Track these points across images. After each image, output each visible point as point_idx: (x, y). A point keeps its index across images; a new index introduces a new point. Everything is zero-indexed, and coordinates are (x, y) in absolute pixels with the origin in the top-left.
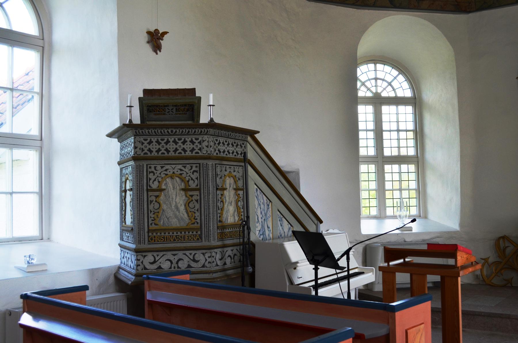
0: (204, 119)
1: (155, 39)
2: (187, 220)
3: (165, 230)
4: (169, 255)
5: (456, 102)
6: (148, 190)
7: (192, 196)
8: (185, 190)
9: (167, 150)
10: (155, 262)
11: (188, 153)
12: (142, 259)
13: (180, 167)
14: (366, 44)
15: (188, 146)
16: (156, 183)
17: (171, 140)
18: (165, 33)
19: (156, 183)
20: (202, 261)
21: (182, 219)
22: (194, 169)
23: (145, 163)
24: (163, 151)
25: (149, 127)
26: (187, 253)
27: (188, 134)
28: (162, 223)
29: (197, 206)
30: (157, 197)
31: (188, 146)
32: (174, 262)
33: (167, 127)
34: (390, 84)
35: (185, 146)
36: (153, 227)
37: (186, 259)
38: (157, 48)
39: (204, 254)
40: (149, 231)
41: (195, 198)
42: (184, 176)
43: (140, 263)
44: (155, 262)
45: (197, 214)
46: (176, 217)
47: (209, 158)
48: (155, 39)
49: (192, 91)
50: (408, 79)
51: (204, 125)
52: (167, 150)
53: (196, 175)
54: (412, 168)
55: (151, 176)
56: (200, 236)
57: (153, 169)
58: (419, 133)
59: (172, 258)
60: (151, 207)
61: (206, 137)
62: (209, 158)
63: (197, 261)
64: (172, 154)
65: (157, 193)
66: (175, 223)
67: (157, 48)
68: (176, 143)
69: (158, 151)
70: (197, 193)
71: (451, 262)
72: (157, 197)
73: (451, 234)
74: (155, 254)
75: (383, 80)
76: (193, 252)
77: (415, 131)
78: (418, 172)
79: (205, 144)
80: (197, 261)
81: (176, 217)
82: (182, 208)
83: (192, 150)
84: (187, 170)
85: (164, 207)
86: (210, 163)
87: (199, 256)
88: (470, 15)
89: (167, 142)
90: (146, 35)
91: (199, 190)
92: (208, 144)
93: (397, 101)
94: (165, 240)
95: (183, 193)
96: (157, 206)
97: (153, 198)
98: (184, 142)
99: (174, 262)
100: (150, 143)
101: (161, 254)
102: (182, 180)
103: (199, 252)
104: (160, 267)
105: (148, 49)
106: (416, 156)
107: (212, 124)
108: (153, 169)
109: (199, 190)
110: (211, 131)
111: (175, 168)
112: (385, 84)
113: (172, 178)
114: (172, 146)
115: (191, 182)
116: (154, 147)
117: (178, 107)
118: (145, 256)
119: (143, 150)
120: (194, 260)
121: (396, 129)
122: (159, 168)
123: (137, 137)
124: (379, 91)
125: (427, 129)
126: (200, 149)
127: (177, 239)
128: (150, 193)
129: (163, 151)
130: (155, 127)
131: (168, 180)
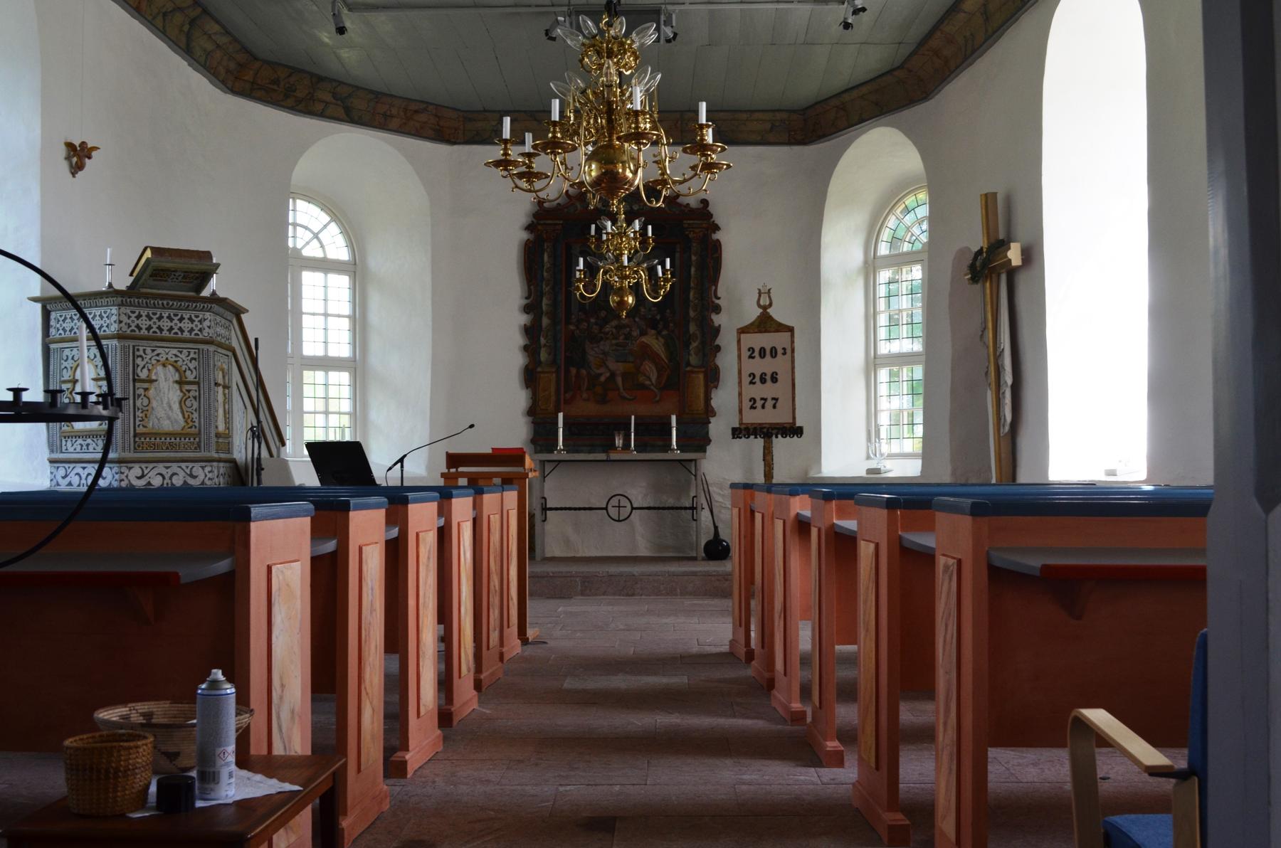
0: (206, 293)
1: (78, 155)
2: (182, 423)
3: (156, 435)
4: (160, 468)
5: (428, 279)
6: (134, 380)
7: (189, 391)
8: (180, 383)
9: (159, 328)
10: (142, 476)
11: (186, 334)
12: (126, 472)
13: (175, 351)
14: (303, 169)
15: (186, 325)
16: (145, 371)
17: (165, 315)
18: (95, 148)
19: (145, 371)
20: (202, 477)
21: (176, 421)
22: (192, 355)
23: (131, 343)
24: (154, 329)
25: (139, 296)
26: (183, 465)
27: (187, 309)
28: (152, 424)
29: (196, 405)
30: (146, 390)
31: (166, 324)
32: (167, 477)
33: (163, 297)
34: (316, 236)
35: (182, 325)
36: (140, 430)
37: (182, 474)
38: (76, 168)
39: (203, 468)
40: (135, 436)
41: (192, 394)
42: (180, 363)
43: (123, 477)
44: (142, 476)
45: (196, 415)
46: (169, 418)
47: (209, 342)
48: (78, 155)
49: (207, 255)
50: (345, 232)
51: (205, 300)
52: (159, 328)
53: (194, 364)
54: (344, 377)
55: (139, 361)
56: (199, 446)
57: (141, 353)
58: (359, 323)
59: (164, 471)
60: (138, 403)
61: (208, 315)
62: (209, 342)
63: (195, 477)
64: (165, 334)
65: (146, 385)
66: (167, 426)
67: (76, 168)
68: (171, 320)
69: (149, 328)
70: (194, 387)
71: (520, 469)
72: (146, 390)
73: (422, 478)
74: (143, 466)
75: (306, 228)
76: (190, 465)
77: (353, 318)
78: (354, 385)
79: (206, 323)
80: (195, 477)
81: (169, 418)
82: (176, 407)
83: (191, 330)
84: (183, 356)
85: (154, 404)
86: (212, 348)
87: (197, 470)
88: (456, 147)
89: (160, 318)
90: (64, 147)
91: (198, 383)
92: (210, 324)
93: (325, 265)
94: (155, 447)
95: (177, 386)
96: (146, 402)
97: (141, 391)
98: (181, 320)
99: (167, 477)
100: (139, 317)
101: (151, 466)
102: (177, 370)
103: (197, 465)
104: (149, 483)
105: (64, 166)
106: (353, 360)
107: (214, 299)
108: (141, 353)
109: (198, 383)
110: (216, 307)
111: (169, 353)
112: (309, 235)
113: (164, 365)
114: (166, 324)
115: (188, 373)
116: (144, 323)
117: (187, 274)
118: (130, 469)
119: (129, 326)
120: (191, 476)
121: (322, 311)
122: (149, 350)
123: (123, 309)
124: (299, 246)
125: (374, 317)
126: (200, 330)
127: (171, 447)
128: (138, 385)
129: (154, 329)
130: (147, 296)
131: (160, 368)
